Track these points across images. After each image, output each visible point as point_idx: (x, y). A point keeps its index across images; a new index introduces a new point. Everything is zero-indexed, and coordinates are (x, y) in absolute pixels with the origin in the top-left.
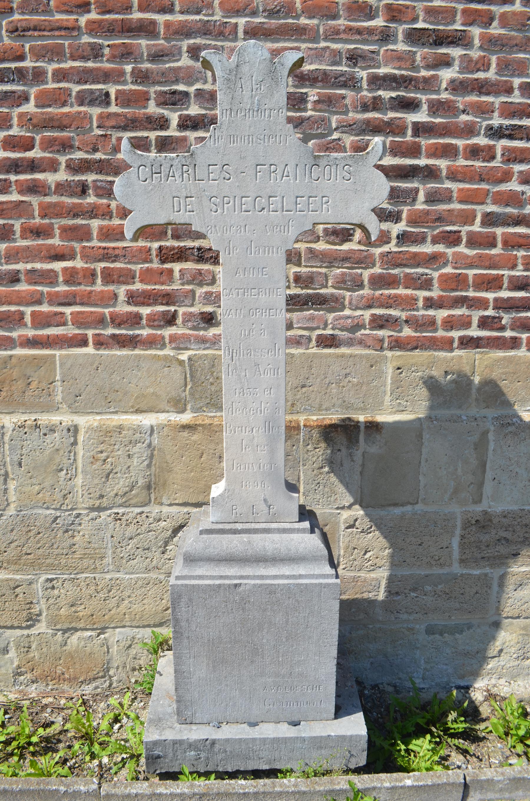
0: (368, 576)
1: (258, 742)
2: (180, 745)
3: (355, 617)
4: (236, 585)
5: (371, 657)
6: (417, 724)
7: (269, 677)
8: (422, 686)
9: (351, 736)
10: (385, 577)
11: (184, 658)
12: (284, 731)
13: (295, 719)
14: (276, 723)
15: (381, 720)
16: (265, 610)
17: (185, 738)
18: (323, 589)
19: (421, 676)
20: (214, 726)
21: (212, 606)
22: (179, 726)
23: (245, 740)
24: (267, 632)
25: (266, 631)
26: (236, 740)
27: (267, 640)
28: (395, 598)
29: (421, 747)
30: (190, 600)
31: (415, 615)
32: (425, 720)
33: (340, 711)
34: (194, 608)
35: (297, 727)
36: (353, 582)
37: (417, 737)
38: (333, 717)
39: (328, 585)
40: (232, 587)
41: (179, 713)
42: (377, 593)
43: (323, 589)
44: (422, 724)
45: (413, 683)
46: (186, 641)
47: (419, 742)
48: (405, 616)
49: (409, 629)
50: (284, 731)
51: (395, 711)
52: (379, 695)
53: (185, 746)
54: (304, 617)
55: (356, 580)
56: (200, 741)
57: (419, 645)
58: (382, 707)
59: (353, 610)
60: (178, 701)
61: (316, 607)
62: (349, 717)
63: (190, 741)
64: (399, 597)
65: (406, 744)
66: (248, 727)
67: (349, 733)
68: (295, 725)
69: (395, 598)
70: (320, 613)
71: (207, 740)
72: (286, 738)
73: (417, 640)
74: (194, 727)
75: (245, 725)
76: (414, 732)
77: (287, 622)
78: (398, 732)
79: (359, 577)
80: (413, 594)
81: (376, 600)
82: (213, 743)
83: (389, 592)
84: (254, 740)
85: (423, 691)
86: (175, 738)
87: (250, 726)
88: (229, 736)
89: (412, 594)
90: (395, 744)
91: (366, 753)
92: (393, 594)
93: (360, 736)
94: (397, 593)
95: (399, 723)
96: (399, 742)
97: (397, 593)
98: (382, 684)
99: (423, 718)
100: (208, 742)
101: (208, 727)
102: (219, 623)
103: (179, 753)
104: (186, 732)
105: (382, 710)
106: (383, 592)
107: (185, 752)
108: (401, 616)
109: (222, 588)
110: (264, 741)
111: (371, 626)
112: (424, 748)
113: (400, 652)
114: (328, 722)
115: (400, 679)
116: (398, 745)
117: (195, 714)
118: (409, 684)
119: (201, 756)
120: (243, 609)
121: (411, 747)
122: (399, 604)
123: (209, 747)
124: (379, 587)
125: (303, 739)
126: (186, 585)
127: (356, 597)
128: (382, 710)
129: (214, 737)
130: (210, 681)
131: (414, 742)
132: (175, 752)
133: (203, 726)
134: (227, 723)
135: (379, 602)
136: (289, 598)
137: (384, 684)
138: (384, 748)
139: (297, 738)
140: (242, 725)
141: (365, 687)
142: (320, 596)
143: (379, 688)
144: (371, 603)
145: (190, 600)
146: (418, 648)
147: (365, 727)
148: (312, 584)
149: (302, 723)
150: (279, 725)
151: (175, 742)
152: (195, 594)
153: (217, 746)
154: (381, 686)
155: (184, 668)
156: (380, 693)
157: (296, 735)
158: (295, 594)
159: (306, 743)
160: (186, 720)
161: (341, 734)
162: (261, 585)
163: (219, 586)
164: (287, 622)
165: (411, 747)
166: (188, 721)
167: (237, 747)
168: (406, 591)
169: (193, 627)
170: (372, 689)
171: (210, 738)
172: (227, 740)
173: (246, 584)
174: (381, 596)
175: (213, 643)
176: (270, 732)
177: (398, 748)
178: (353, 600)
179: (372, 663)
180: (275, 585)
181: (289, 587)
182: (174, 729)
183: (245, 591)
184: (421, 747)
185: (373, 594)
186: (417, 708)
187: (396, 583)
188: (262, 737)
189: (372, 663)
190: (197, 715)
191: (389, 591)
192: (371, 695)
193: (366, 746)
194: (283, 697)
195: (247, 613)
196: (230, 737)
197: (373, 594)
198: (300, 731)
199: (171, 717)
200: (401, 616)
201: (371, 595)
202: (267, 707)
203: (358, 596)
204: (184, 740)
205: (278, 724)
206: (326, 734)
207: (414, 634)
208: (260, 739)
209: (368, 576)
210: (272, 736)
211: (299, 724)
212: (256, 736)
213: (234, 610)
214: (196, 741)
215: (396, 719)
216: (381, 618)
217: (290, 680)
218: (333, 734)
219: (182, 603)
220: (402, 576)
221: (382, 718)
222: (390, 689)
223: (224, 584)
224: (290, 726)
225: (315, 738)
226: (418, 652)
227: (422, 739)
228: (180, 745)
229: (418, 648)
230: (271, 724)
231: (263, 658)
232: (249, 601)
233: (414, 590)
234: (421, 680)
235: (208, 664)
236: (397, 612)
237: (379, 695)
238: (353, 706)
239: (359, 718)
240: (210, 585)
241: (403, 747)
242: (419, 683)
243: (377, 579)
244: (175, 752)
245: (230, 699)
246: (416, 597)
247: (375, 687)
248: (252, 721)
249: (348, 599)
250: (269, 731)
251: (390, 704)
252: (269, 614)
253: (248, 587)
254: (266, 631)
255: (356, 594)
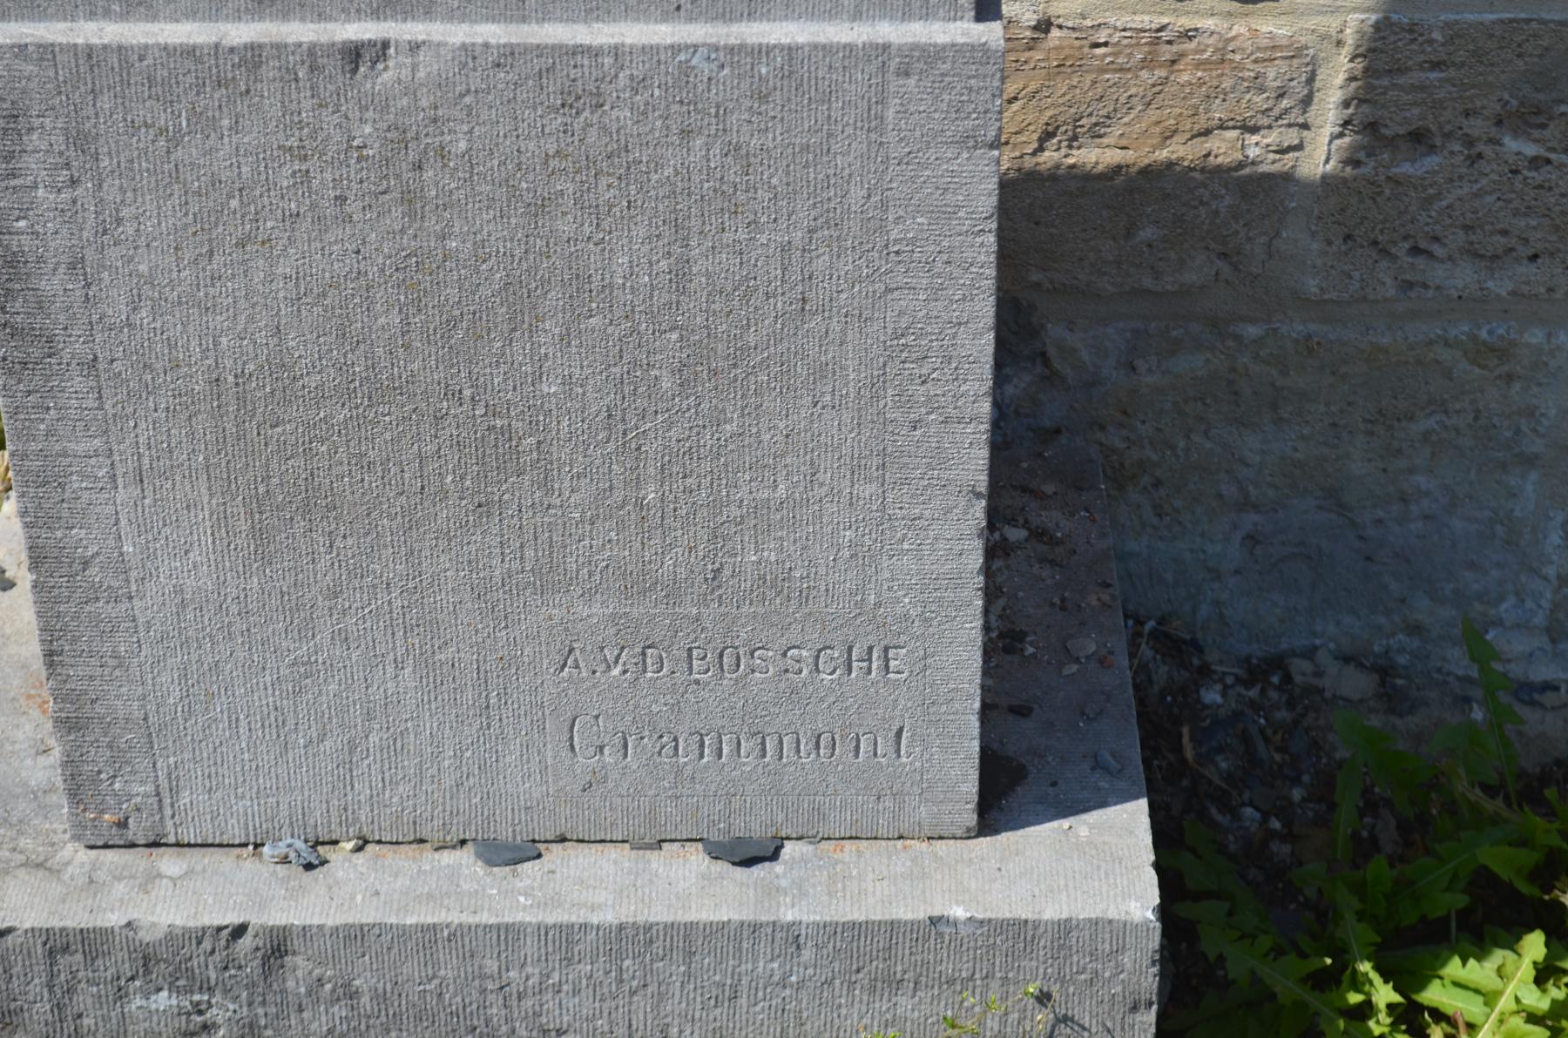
0: (1240, 28)
1: (530, 948)
2: (91, 957)
3: (1157, 275)
4: (354, 54)
5: (1246, 504)
6: (1483, 880)
7: (588, 596)
8: (1543, 672)
9: (1065, 928)
10: (1350, 36)
11: (75, 482)
12: (689, 888)
13: (755, 827)
14: (640, 846)
15: (1281, 850)
16: (541, 207)
17: (114, 919)
18: (894, 84)
19: (1539, 620)
20: (285, 860)
21: (215, 182)
22: (85, 856)
23: (457, 934)
24: (565, 339)
25: (552, 327)
26: (402, 934)
27: (567, 381)
28: (1406, 168)
29: (1489, 998)
30: (81, 141)
31: (1526, 270)
32: (1528, 858)
33: (1008, 792)
34: (111, 192)
35: (758, 871)
36: (1148, 63)
37: (1478, 942)
38: (971, 819)
39: (930, 55)
40: (332, 66)
41: (78, 786)
42: (1292, 137)
43: (894, 84)
44: (1504, 875)
45: (1482, 653)
46: (78, 382)
47: (1478, 971)
48: (1464, 277)
49: (1481, 352)
50: (689, 888)
51: (1371, 805)
52: (1282, 715)
53: (119, 962)
54: (785, 248)
55: (1166, 53)
56: (199, 935)
57: (1537, 446)
58: (1296, 781)
59: (1147, 233)
60: (68, 725)
61: (857, 194)
62: (1065, 823)
63: (145, 936)
64: (1432, 162)
65: (1408, 978)
66: (480, 869)
67: (1052, 911)
68: (748, 862)
69: (1406, 168)
70: (882, 229)
71: (240, 931)
72: (689, 927)
73: (1530, 412)
74: (170, 864)
75: (465, 858)
76: (1464, 915)
77: (680, 277)
78: (1361, 916)
79: (1187, 35)
80: (1517, 146)
81: (1287, 177)
82: (278, 947)
83: (1371, 127)
84: (508, 934)
85: (1548, 698)
86: (56, 923)
87: (491, 863)
88: (367, 914)
89: (1511, 144)
90: (1339, 976)
91: (1150, 1017)
92: (1391, 142)
93: (1120, 930)
94: (1419, 139)
95: (1378, 868)
96: (1365, 967)
97: (1419, 139)
98: (1310, 654)
99: (1523, 843)
100: (246, 942)
101: (250, 865)
102: (270, 279)
103: (84, 999)
104: (120, 888)
105: (1297, 794)
106: (1329, 130)
107: (121, 995)
108: (1437, 274)
109: (269, 71)
110: (564, 940)
111: (1253, 331)
112: (1505, 1003)
113: (1422, 480)
114: (940, 846)
115: (1415, 629)
116: (1358, 983)
117: (175, 791)
118: (1458, 661)
119: (215, 1014)
120: (409, 199)
121: (1434, 995)
122: (1429, 200)
123: (253, 968)
124: (1307, 101)
125: (791, 938)
126: (47, 52)
127: (1163, 155)
128: (1297, 794)
129: (279, 916)
130: (244, 614)
131: (1454, 968)
132: (62, 996)
133: (224, 861)
134: (362, 844)
135: (1306, 186)
136: (686, 133)
137: (1323, 657)
138: (1272, 997)
139: (755, 927)
140: (447, 857)
141: (1205, 671)
142: (875, 124)
143: (1287, 678)
144: (1260, 191)
145: (81, 141)
146: (1529, 461)
147: (1152, 877)
148: (827, 49)
149: (789, 849)
150: (656, 861)
151: (56, 944)
152: (105, 102)
153: (300, 967)
154: (1300, 669)
155: (86, 539)
156: (1291, 704)
157: (747, 915)
158: (722, 112)
159: (807, 954)
160: (123, 824)
161: (1006, 913)
162: (509, 55)
163: (252, 56)
164: (680, 277)
165: (1434, 995)
166: (135, 831)
167: (411, 969)
168: (1477, 127)
169: (117, 309)
170: (1248, 684)
171: (256, 919)
172: (355, 935)
173: (415, 47)
174: (1320, 154)
175: (241, 400)
176: (601, 897)
177: (1354, 998)
178: (1146, 171)
179: (1252, 539)
180: (594, 52)
181: (686, 70)
182: (55, 872)
183: (411, 91)
184: (1489, 998)
185: (1272, 138)
186: (1490, 790)
187: (1415, 77)
188: (551, 918)
189: (1252, 539)
190: (185, 799)
191: (1369, 124)
192: (1237, 715)
193: (1149, 982)
194: (676, 707)
195: (432, 224)
196: (368, 916)
197: (1272, 138)
198: (771, 891)
199: (45, 811)
200: (1437, 274)
201: (1255, 146)
202: (585, 762)
203: (1180, 151)
204: (107, 933)
205: (653, 856)
206: (922, 914)
207: (1510, 378)
208: (543, 930)
209: (1240, 28)
210: (609, 917)
211: (774, 856)
212: (520, 917)
213: (352, 207)
214: (173, 938)
215: (1364, 848)
216: (1312, 285)
217: (711, 611)
218: (960, 913)
219: (30, 161)
220: (1455, 34)
221: (1288, 836)
222: (1355, 683)
223: (280, 48)
224: (722, 867)
225: (857, 930)
226: (1530, 485)
227: (1499, 956)
228: (91, 957)
229: (1529, 461)
230: (612, 852)
231: (545, 484)
232: (442, 153)
233: (1527, 118)
234: (1541, 641)
235: (222, 520)
236: (1416, 251)
237: (1282, 715)
238: (1097, 765)
239: (1127, 826)
240: (190, 52)
241: (1385, 994)
242: (1521, 651)
243: (1299, 52)
244: (62, 996)
245: (369, 716)
246: (1535, 162)
247: (1266, 669)
248: (505, 833)
249: (1118, 169)
250: (592, 887)
251: (1340, 764)
252: (565, 227)
253: (427, 65)
254: (552, 327)
255: (1166, 137)
